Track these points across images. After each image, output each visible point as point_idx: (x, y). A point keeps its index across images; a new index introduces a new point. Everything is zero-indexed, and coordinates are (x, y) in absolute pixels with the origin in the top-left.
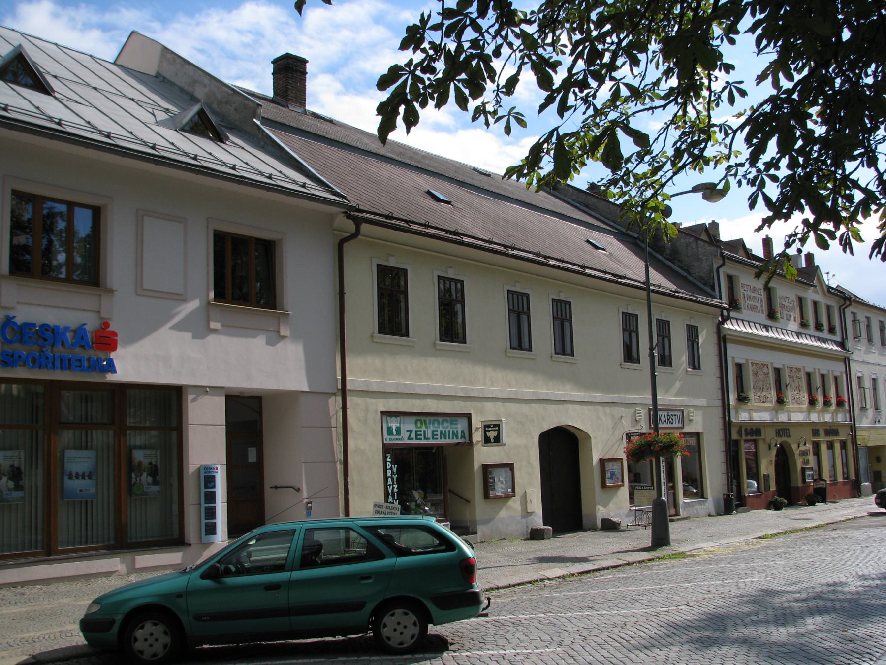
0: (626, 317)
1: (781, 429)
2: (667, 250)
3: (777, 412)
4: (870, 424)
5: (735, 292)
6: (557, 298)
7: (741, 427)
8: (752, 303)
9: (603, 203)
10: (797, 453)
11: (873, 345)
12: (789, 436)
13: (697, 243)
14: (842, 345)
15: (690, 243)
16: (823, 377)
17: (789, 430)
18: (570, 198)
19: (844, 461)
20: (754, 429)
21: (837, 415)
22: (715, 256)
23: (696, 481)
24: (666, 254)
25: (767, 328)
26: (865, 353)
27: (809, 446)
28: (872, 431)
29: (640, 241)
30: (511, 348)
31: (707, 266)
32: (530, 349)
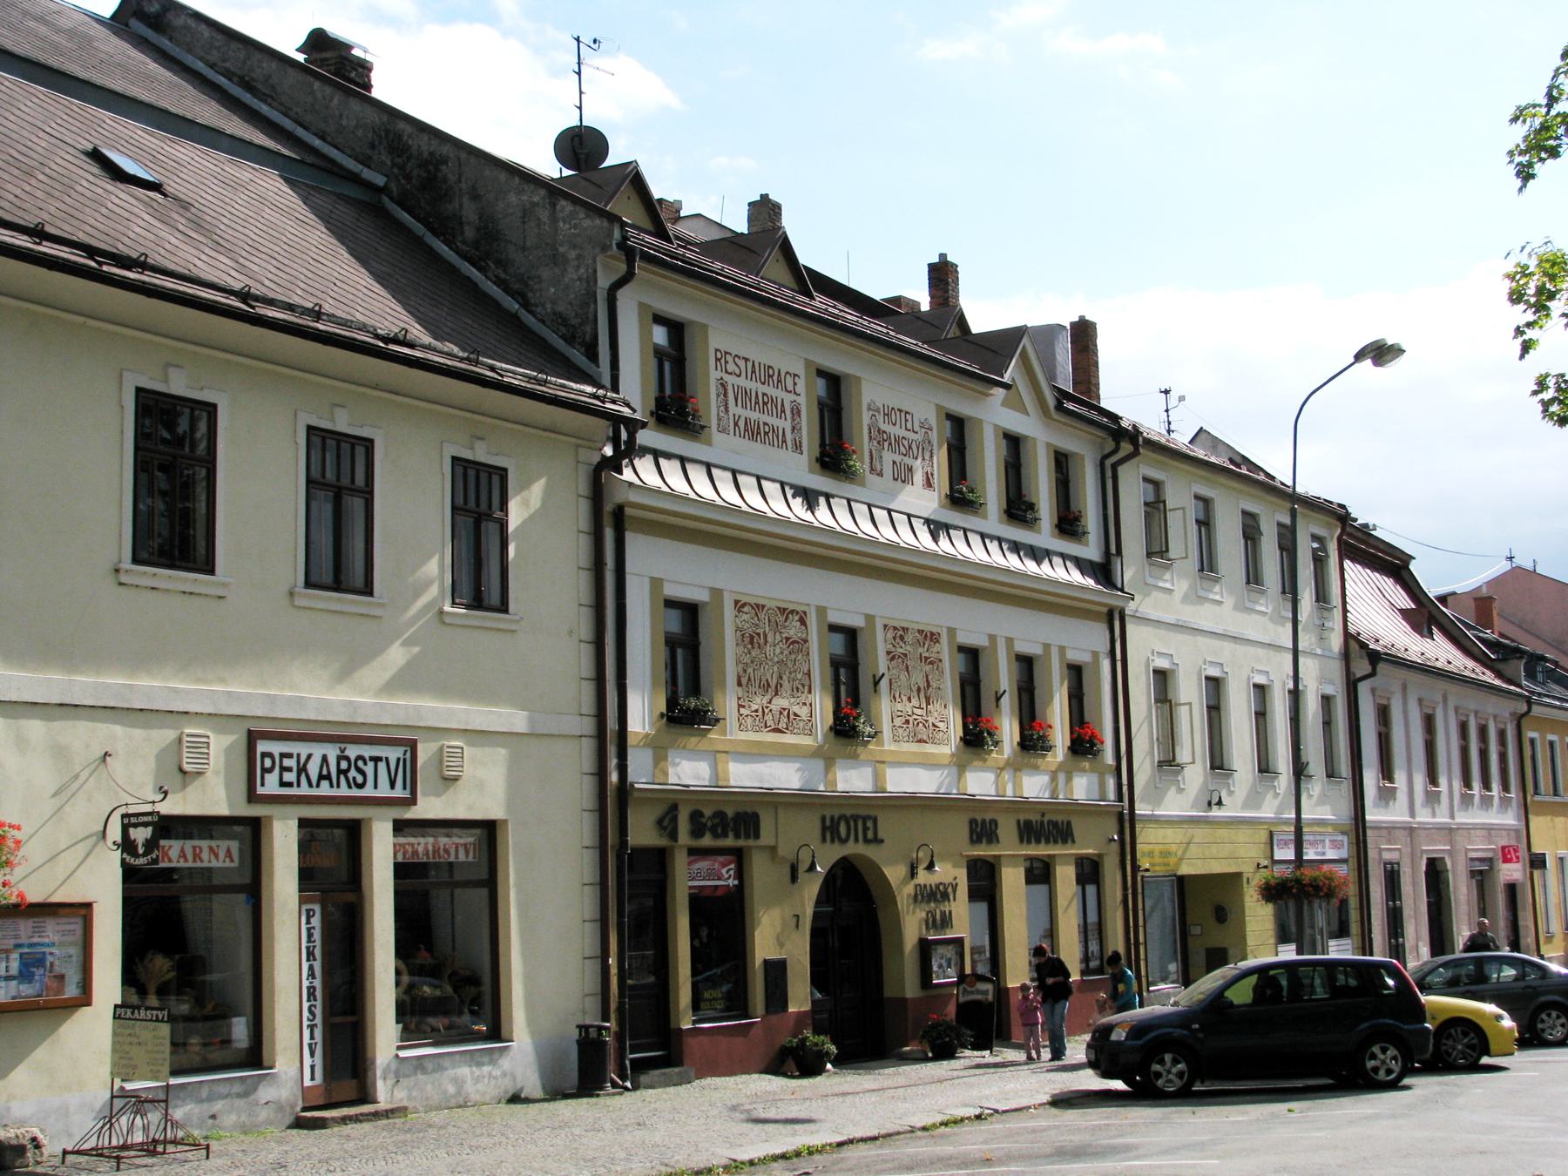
0: (465, 475)
1: (842, 817)
2: (466, 228)
3: (829, 762)
5: (1071, 491)
6: (325, 424)
7: (673, 808)
8: (754, 416)
9: (355, 105)
10: (904, 893)
11: (1217, 580)
12: (877, 840)
13: (554, 205)
14: (1103, 571)
15: (534, 205)
16: (1026, 664)
17: (875, 820)
18: (201, 59)
19: (1092, 917)
20: (730, 813)
21: (1069, 779)
22: (605, 248)
23: (474, 981)
24: (464, 242)
25: (810, 498)
26: (1186, 599)
27: (952, 872)
28: (1199, 833)
29: (392, 199)
30: (309, 584)
31: (580, 279)
32: (503, 608)
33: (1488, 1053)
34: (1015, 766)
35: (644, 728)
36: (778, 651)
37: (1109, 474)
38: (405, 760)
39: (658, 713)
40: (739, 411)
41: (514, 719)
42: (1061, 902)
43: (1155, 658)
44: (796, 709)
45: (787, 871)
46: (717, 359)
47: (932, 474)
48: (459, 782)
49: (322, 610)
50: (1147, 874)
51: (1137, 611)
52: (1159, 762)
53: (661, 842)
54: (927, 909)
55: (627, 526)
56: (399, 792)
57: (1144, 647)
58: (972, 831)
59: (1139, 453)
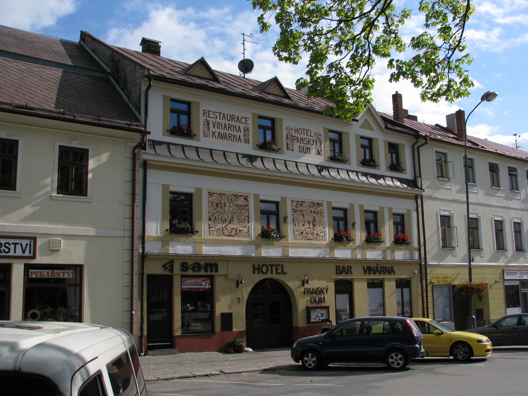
7: (172, 262)
12: (283, 273)
17: (283, 266)
18: (89, 47)
33: (473, 356)
34: (362, 248)
35: (157, 234)
37: (416, 150)
38: (30, 244)
41: (91, 231)
42: (387, 294)
43: (441, 211)
44: (241, 229)
46: (204, 113)
47: (321, 150)
49: (61, 200)
51: (431, 196)
52: (442, 247)
53: (167, 273)
54: (311, 297)
56: (27, 254)
57: (428, 206)
58: (337, 270)
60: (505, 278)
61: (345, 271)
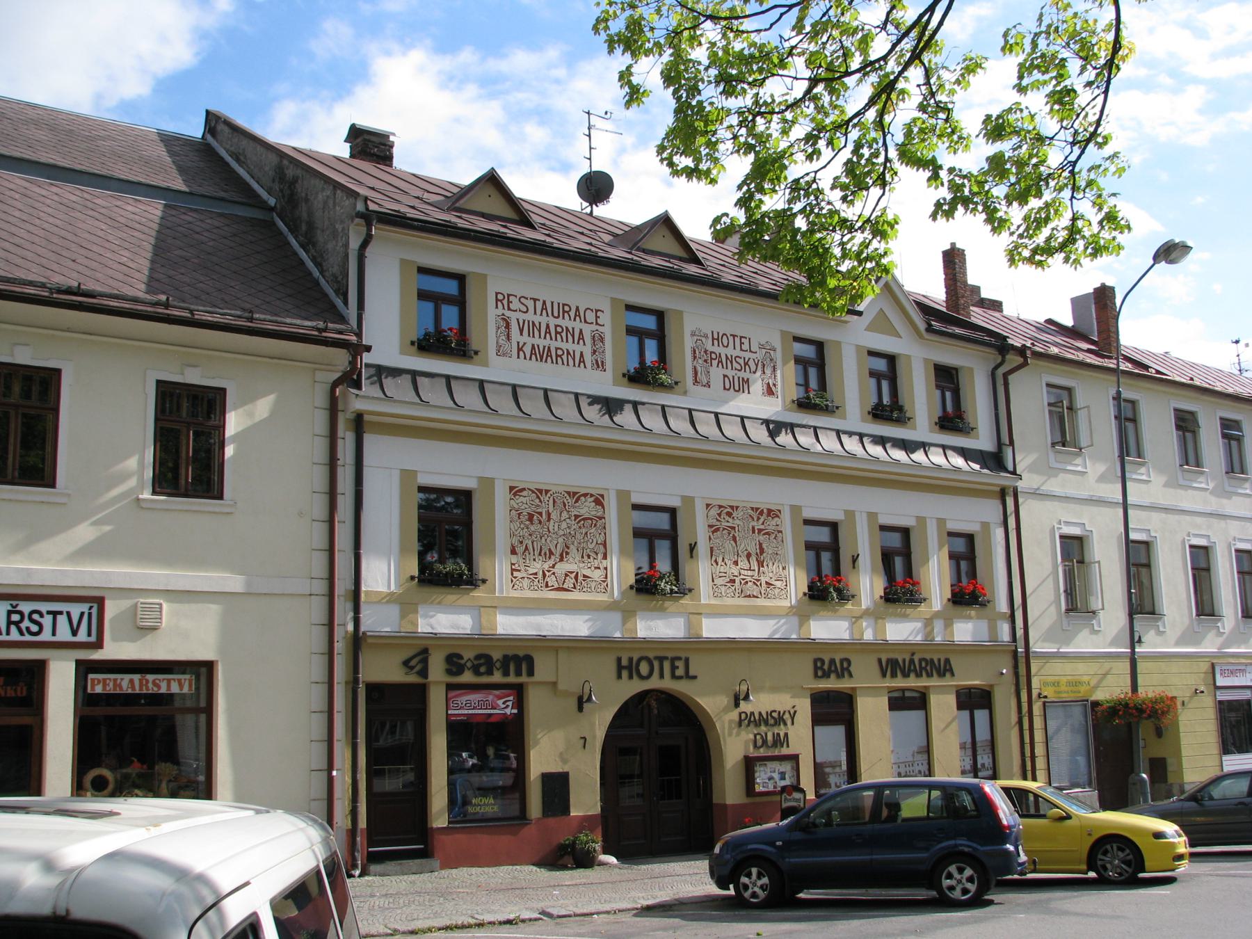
4: (1112, 644)
36: (564, 525)
37: (1000, 382)
38: (90, 614)
39: (408, 575)
40: (525, 338)
41: (233, 582)
43: (1062, 526)
45: (573, 703)
46: (497, 300)
48: (158, 631)
50: (1046, 700)
51: (1038, 489)
53: (413, 678)
55: (365, 429)
56: (82, 636)
58: (816, 669)
59: (1028, 364)
60: (1218, 684)
61: (915, 670)
